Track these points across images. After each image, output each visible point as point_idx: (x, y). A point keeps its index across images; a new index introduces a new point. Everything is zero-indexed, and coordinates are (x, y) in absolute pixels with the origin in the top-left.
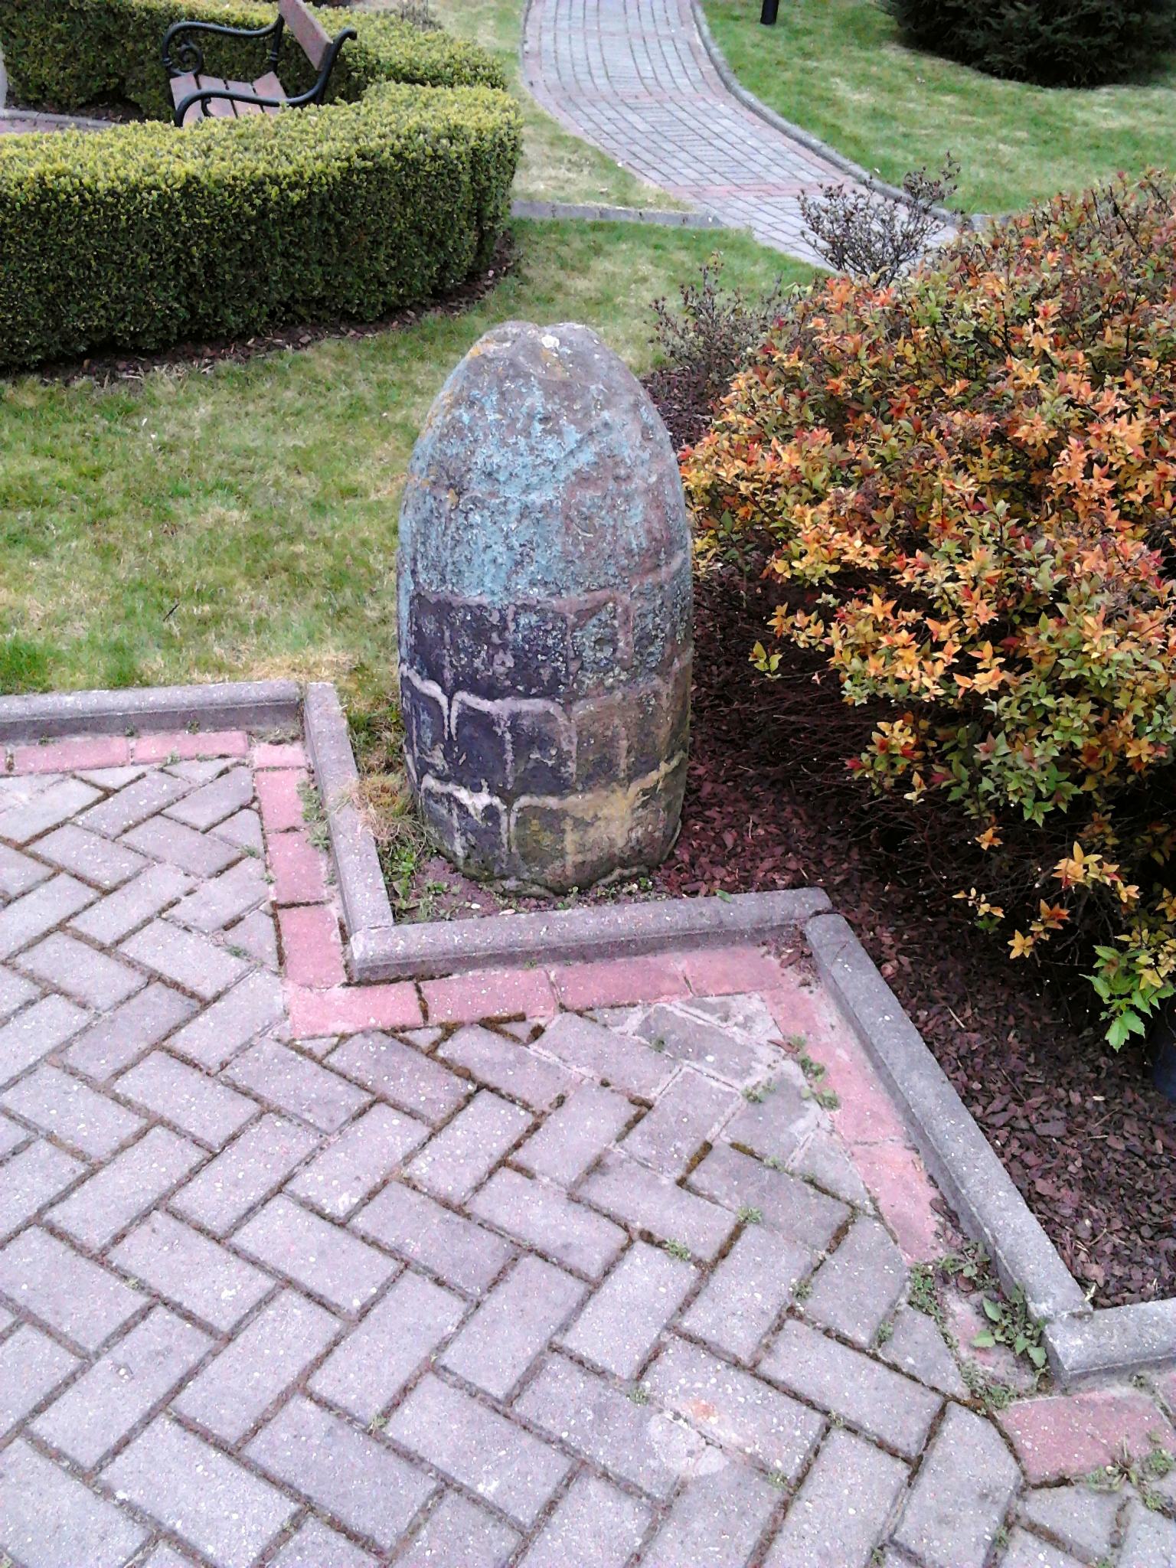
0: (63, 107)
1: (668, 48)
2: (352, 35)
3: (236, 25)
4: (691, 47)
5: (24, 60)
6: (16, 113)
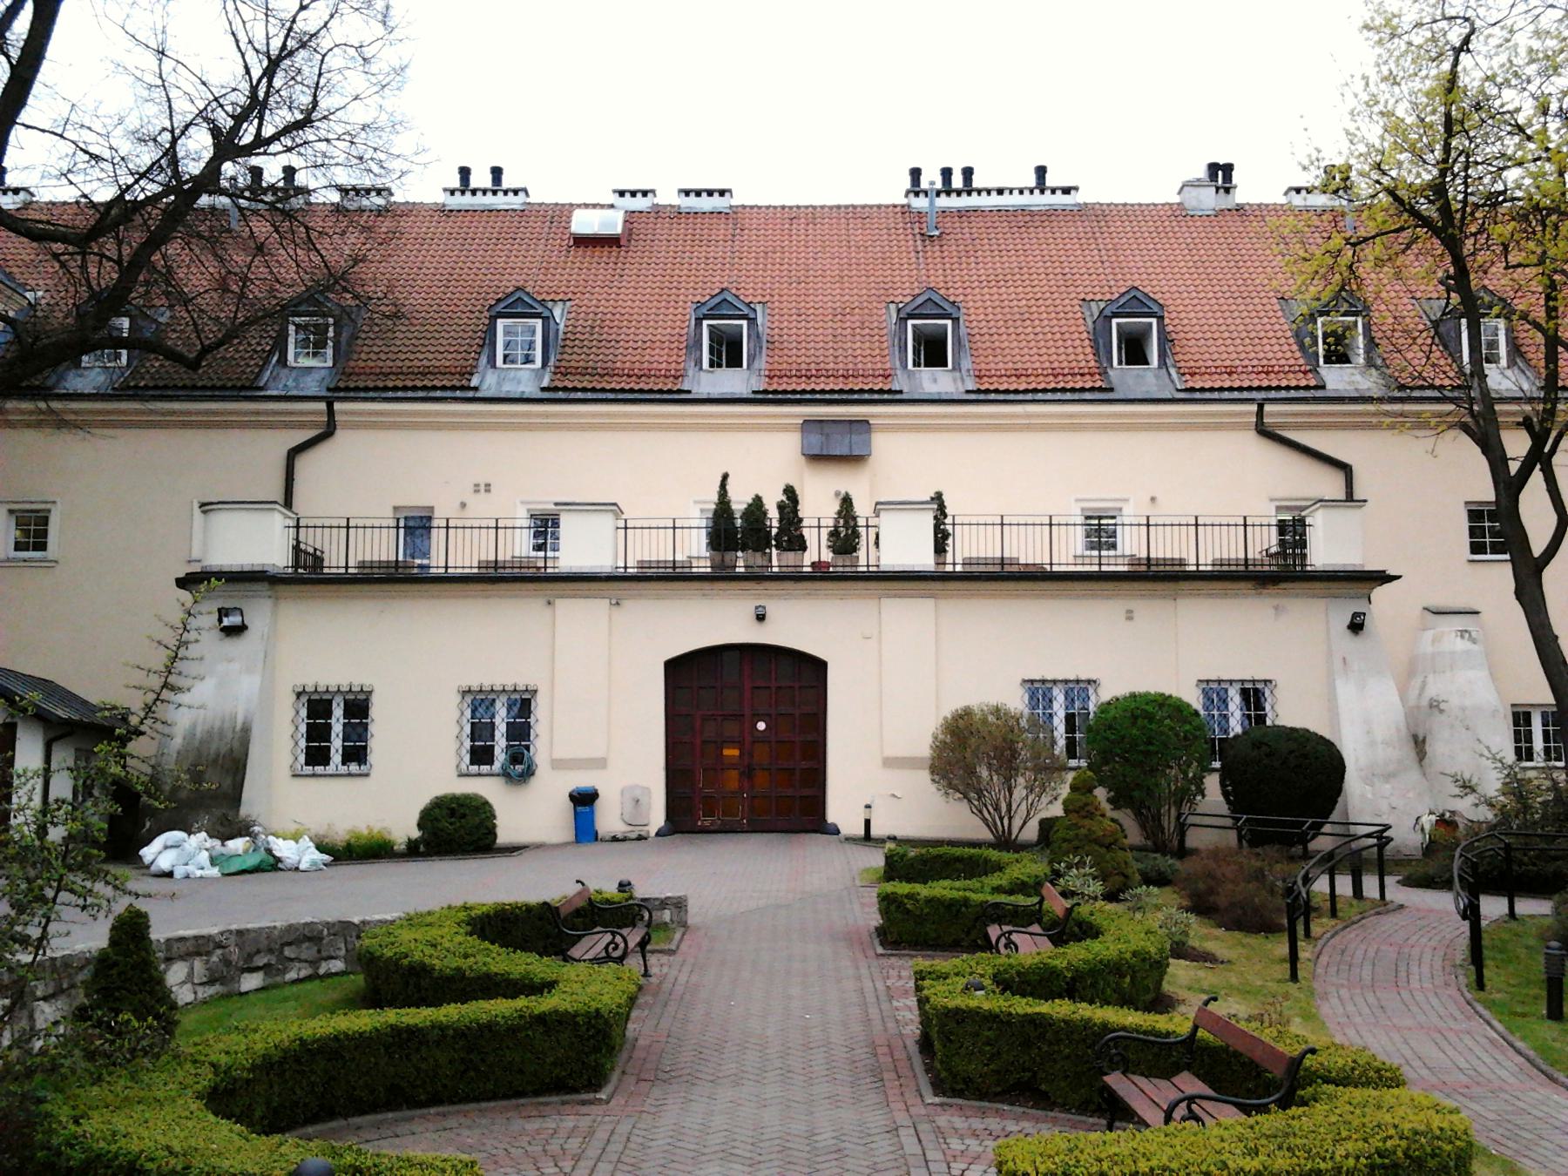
0: (982, 1096)
1: (1467, 1040)
2: (1313, 1051)
3: (1145, 1033)
4: (1492, 1041)
5: (956, 1059)
6: (945, 1100)
